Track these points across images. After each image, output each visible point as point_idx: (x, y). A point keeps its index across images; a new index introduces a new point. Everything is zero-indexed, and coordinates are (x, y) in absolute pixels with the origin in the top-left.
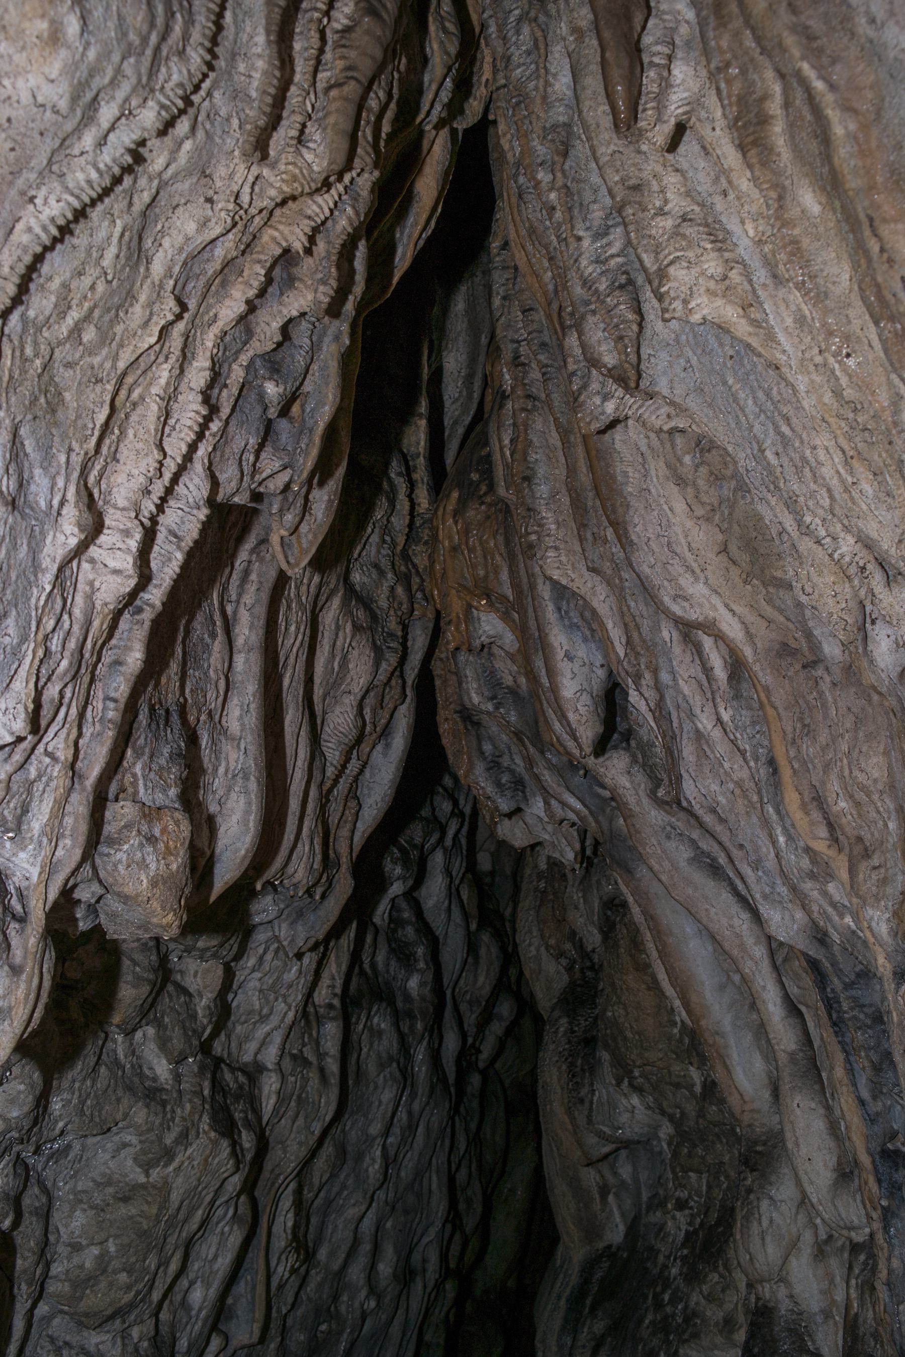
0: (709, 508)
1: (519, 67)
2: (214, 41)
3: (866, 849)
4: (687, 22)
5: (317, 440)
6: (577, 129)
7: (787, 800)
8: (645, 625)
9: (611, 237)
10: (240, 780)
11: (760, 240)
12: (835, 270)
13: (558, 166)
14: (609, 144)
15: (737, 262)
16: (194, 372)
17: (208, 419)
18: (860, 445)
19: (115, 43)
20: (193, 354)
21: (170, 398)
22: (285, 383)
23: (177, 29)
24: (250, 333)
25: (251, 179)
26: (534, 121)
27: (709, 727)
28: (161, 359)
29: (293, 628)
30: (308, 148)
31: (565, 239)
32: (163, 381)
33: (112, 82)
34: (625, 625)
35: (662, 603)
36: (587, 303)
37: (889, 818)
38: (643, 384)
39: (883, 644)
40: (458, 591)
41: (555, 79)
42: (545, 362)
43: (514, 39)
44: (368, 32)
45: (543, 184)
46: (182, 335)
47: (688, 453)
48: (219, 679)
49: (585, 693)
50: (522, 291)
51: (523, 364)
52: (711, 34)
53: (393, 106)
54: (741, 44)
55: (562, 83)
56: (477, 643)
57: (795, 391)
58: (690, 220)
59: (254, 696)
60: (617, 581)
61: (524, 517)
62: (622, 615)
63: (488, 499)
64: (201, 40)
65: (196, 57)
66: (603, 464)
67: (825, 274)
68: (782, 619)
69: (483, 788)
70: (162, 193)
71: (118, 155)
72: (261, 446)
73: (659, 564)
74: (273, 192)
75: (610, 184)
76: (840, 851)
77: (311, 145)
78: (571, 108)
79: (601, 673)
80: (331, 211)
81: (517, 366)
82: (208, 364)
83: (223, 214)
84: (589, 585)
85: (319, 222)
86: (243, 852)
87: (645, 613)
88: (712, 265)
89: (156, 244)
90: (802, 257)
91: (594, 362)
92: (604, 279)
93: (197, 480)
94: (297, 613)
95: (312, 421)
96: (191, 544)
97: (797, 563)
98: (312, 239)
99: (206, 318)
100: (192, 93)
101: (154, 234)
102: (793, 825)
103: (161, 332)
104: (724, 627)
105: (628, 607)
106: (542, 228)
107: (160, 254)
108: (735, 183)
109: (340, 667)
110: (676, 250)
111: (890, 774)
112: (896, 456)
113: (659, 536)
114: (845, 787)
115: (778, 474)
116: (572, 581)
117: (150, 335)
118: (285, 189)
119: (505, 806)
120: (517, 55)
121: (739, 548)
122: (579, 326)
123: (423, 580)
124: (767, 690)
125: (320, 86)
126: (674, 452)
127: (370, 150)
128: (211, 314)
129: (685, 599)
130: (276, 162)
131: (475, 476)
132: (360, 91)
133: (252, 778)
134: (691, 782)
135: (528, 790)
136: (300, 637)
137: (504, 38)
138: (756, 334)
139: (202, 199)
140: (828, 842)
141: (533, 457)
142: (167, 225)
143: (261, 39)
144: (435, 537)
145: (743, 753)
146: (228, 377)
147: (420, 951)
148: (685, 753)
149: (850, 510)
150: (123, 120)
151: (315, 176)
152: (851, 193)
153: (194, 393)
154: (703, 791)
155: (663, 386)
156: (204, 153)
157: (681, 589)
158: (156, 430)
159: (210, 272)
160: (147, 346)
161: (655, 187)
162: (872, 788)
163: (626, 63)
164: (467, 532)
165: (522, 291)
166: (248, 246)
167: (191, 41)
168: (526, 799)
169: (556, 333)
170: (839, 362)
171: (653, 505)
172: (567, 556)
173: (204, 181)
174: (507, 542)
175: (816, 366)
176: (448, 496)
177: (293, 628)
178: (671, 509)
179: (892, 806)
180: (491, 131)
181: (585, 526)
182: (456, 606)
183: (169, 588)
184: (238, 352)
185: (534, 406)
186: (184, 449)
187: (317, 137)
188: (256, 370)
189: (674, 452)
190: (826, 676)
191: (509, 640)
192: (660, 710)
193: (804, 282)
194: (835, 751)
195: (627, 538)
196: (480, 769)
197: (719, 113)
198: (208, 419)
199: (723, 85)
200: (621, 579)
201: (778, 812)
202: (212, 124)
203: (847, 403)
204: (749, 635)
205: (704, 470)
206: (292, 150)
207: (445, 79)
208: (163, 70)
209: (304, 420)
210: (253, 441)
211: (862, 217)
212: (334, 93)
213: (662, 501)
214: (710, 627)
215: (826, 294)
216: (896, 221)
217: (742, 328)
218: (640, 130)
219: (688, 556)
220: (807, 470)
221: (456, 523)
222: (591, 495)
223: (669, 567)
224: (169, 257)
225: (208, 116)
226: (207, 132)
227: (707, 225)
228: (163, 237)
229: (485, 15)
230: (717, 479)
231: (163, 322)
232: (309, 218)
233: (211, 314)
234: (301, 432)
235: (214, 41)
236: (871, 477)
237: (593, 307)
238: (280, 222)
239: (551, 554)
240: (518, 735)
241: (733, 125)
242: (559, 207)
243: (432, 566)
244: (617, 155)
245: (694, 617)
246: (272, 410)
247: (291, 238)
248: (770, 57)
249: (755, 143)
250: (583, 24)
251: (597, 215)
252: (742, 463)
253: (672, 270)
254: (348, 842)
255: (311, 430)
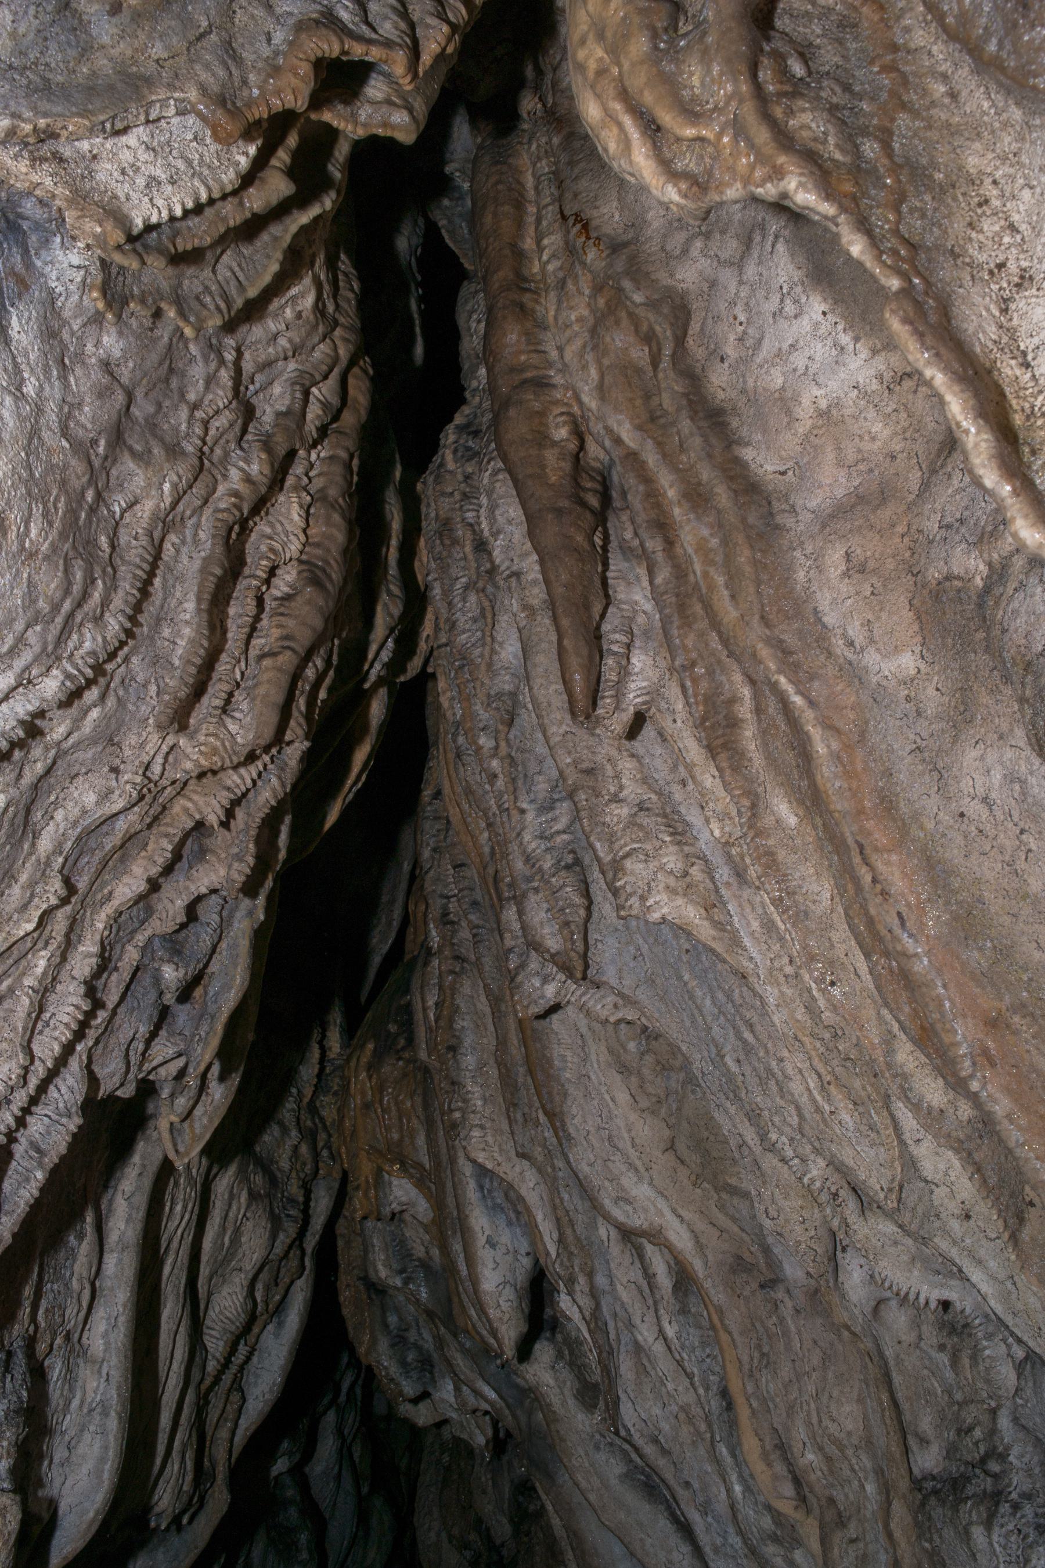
0: (654, 1099)
1: (464, 632)
2: (138, 608)
3: (839, 1514)
4: (644, 612)
5: (220, 1028)
6: (525, 698)
7: (746, 1447)
8: (580, 1219)
9: (557, 812)
10: (97, 1417)
11: (727, 843)
12: (815, 887)
13: (502, 736)
14: (561, 724)
15: (699, 858)
16: (79, 957)
17: (90, 1015)
18: (839, 1070)
19: (20, 610)
20: (80, 936)
21: (46, 990)
22: (187, 966)
23: (96, 596)
24: (150, 911)
25: (165, 748)
26: (478, 686)
27: (651, 1340)
28: (40, 944)
29: (179, 1208)
30: (233, 717)
31: (508, 809)
32: (39, 970)
33: (11, 651)
34: (558, 1220)
35: (602, 1206)
36: (529, 880)
37: (866, 1479)
38: (591, 972)
39: (855, 1275)
40: (368, 1153)
41: (502, 648)
42: (477, 922)
43: (460, 605)
44: (309, 602)
45: (485, 750)
46: (68, 918)
47: (633, 1039)
48: (83, 1288)
49: (508, 1286)
50: (454, 845)
51: (452, 923)
52: (675, 632)
53: (331, 673)
54: (707, 645)
55: (510, 651)
56: (387, 1211)
57: (764, 1004)
58: (648, 809)
59: (125, 1306)
60: (549, 1170)
61: (447, 1092)
62: (555, 1208)
63: (406, 1055)
64: (122, 607)
65: (114, 624)
66: (538, 1045)
67: (804, 890)
68: (736, 1229)
69: (386, 1368)
70: (59, 762)
71: (8, 727)
72: (153, 1035)
73: (599, 1161)
74: (188, 765)
75: (562, 765)
76: (808, 1512)
77: (237, 715)
78: (518, 677)
79: (526, 1262)
80: (254, 782)
81: (445, 924)
82: (95, 949)
83: (128, 787)
84: (517, 1169)
85: (239, 794)
86: (91, 1514)
87: (580, 1208)
88: (672, 860)
89: (47, 817)
90: (778, 870)
91: (535, 945)
92: (549, 857)
93: (71, 1081)
94: (185, 1189)
95: (214, 1006)
96: (57, 1161)
97: (760, 1182)
98: (230, 814)
99: (99, 896)
100: (105, 662)
101: (45, 805)
102: (751, 1475)
103: (41, 918)
104: (672, 1236)
105: (562, 1200)
106: (480, 792)
107: (51, 827)
108: (699, 778)
109: (231, 1242)
110: (633, 841)
111: (867, 1427)
112: (883, 1091)
113: (599, 1128)
114: (813, 1437)
115: (740, 1084)
116: (499, 1165)
117: (29, 921)
118: (203, 762)
119: (409, 1389)
120: (462, 620)
121: (689, 1147)
122: (520, 900)
123: (330, 1136)
124: (720, 1311)
125: (253, 653)
126: (617, 1037)
127: (302, 721)
128: (106, 891)
129: (628, 1202)
130: (196, 731)
131: (393, 1028)
132: (295, 661)
133: (113, 1414)
134: (630, 1404)
135: (436, 1370)
136: (187, 1216)
137: (450, 604)
138: (721, 939)
139: (106, 769)
140: (794, 1503)
141: (459, 1023)
142: (62, 795)
143: (190, 606)
144: (345, 1087)
145: (690, 1376)
146: (120, 959)
147: (303, 1538)
148: (623, 1369)
149: (822, 1132)
150: (21, 689)
151: (238, 749)
152: (836, 815)
153: (75, 983)
154: (643, 1415)
155: (610, 975)
156: (113, 720)
157: (623, 1190)
158: (25, 1029)
159: (108, 847)
160: (22, 933)
161: (609, 770)
162: (845, 1442)
163: (585, 652)
164: (381, 1089)
165: (454, 845)
166: (156, 818)
167: (111, 607)
168: (433, 1381)
169: (491, 899)
170: (823, 991)
171: (593, 1093)
172: (493, 1136)
173: (110, 749)
174: (426, 1106)
175: (786, 976)
176: (362, 1046)
177: (179, 1208)
178: (613, 1100)
179: (869, 1465)
180: (430, 685)
181: (515, 1105)
182: (366, 1168)
183: (23, 1215)
184: (134, 931)
185: (463, 968)
186: (57, 1049)
187: (244, 706)
188: (153, 951)
189: (617, 1037)
190: (787, 1300)
191: (423, 1208)
192: (595, 1320)
193: (781, 899)
194: (800, 1390)
195: (564, 1131)
196: (383, 1344)
197: (680, 706)
198: (90, 1015)
199: (689, 684)
200: (553, 1167)
201: (734, 1456)
202: (126, 690)
203: (826, 1027)
204: (699, 1245)
205: (649, 1059)
206: (215, 720)
207: (386, 641)
208: (75, 637)
209: (205, 1003)
210: (143, 1030)
211: (850, 841)
212: (267, 662)
213: (603, 1089)
214: (656, 1236)
215: (806, 913)
216: (889, 851)
217: (705, 932)
218: (598, 718)
219: (631, 1152)
220: (773, 1082)
221: (370, 1077)
222: (522, 1070)
223: (610, 1164)
224: (61, 831)
225: (123, 681)
226: (119, 699)
227: (665, 816)
228: (56, 809)
229: (430, 578)
230: (664, 1068)
231: (44, 906)
232: (229, 789)
233: (106, 891)
234: (201, 1016)
235: (138, 608)
236: (851, 1106)
237: (536, 884)
238: (195, 791)
239: (476, 1133)
240: (430, 1314)
241: (700, 724)
242: (501, 776)
243: (342, 1119)
244: (569, 736)
245: (637, 1223)
246: (169, 996)
247: (206, 810)
248: (739, 661)
249: (725, 746)
250: (535, 602)
251: (542, 786)
252: (697, 1064)
253: (628, 864)
254: (226, 1444)
255: (213, 1017)
